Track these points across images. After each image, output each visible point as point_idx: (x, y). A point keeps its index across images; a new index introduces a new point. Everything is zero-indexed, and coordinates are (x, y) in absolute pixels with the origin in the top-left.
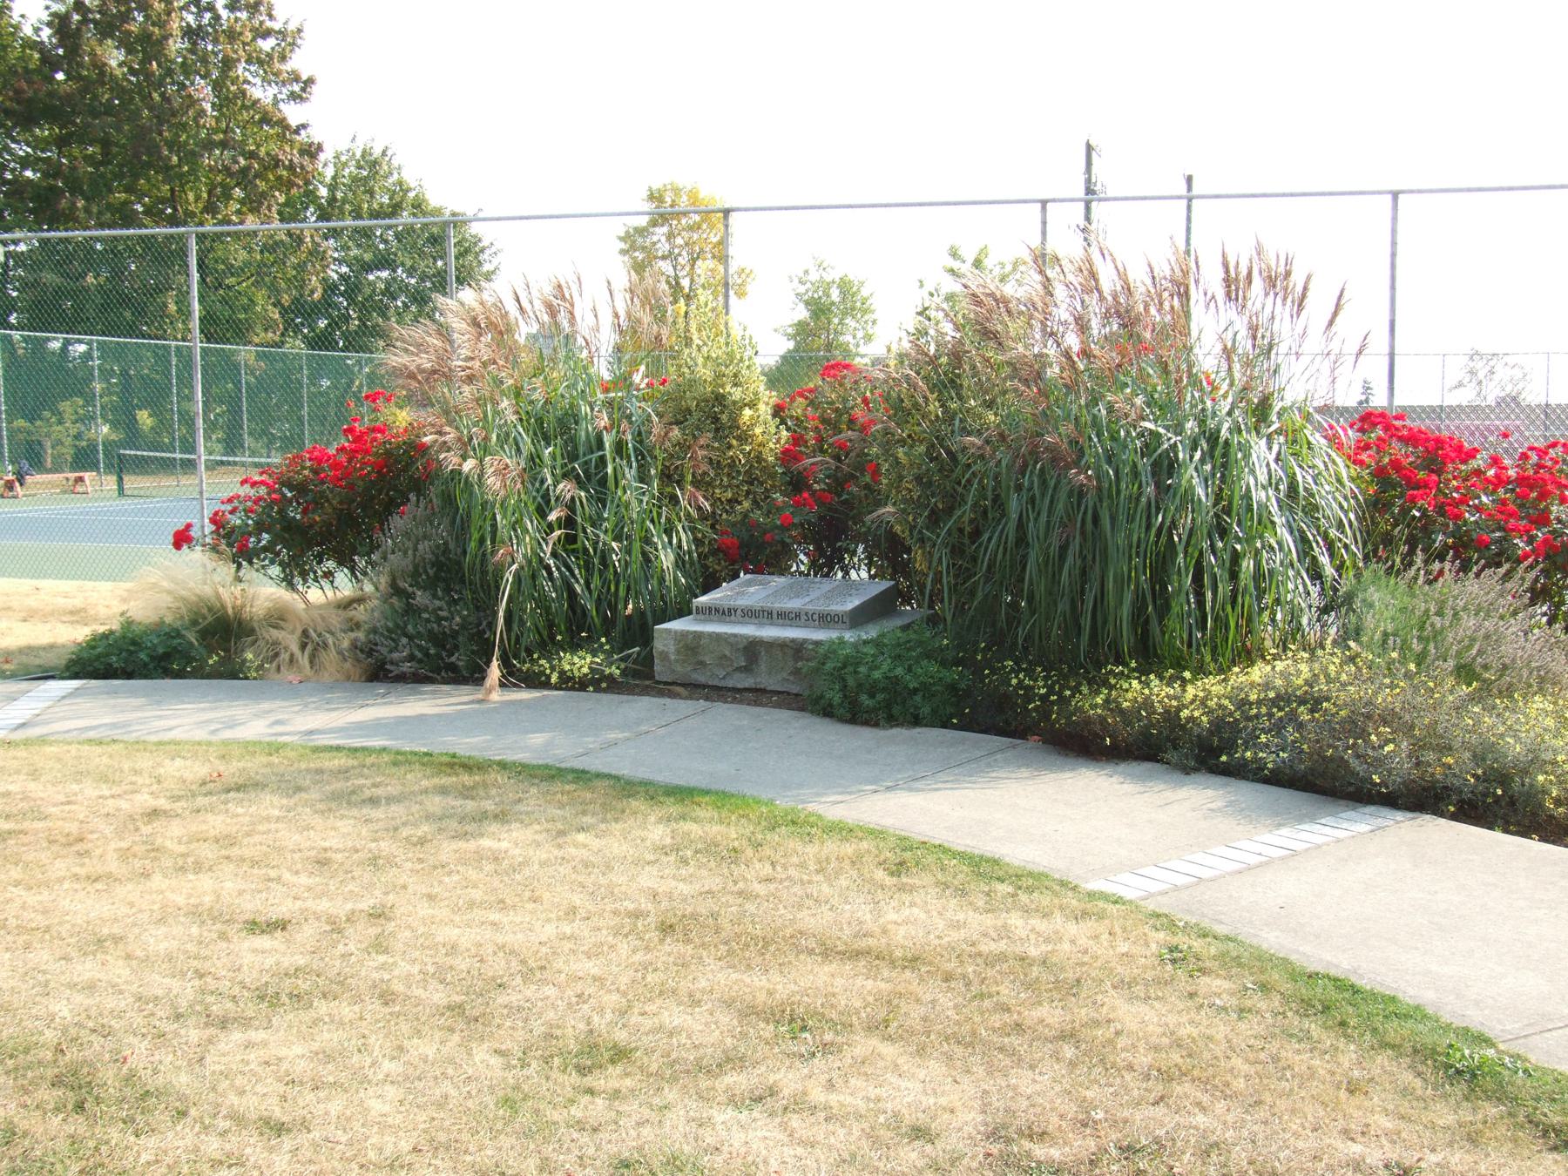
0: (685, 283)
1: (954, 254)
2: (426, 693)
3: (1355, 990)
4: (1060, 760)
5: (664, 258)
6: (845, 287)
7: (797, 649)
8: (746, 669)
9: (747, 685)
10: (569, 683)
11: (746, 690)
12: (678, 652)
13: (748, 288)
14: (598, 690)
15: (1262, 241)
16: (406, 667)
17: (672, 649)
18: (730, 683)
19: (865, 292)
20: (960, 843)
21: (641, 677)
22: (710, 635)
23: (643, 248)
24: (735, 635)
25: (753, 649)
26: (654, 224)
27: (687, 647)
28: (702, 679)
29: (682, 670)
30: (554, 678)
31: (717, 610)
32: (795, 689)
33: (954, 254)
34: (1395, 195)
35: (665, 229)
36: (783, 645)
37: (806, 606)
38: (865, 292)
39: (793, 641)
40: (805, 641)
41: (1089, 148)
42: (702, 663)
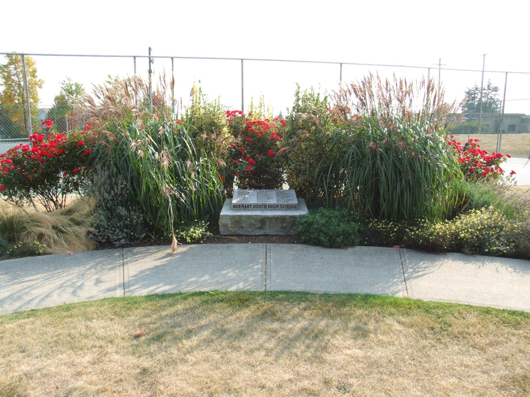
0: (22, 83)
1: (109, 77)
2: (137, 254)
3: (471, 307)
4: (422, 255)
5: (14, 75)
6: (77, 86)
7: (283, 219)
8: (261, 228)
9: (260, 234)
10: (195, 241)
11: (260, 235)
12: (232, 223)
13: (43, 86)
14: (205, 242)
15: (371, 73)
16: (123, 241)
17: (229, 222)
18: (253, 234)
19: (83, 87)
20: (476, 301)
21: (216, 235)
22: (246, 216)
23: (7, 72)
24: (256, 216)
25: (263, 221)
26: (10, 64)
27: (235, 221)
28: (242, 233)
29: (233, 230)
30: (189, 240)
31: (243, 206)
32: (281, 234)
33: (109, 77)
34: (341, 64)
35: (13, 66)
36: (276, 218)
37: (281, 201)
38: (83, 87)
39: (281, 216)
40: (286, 216)
41: (150, 49)
42: (242, 227)
